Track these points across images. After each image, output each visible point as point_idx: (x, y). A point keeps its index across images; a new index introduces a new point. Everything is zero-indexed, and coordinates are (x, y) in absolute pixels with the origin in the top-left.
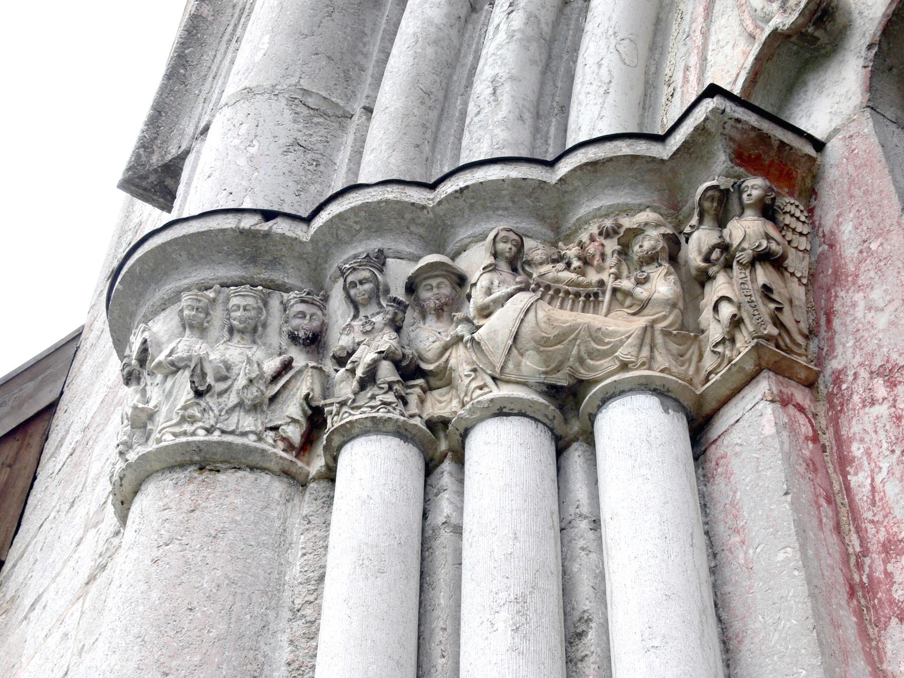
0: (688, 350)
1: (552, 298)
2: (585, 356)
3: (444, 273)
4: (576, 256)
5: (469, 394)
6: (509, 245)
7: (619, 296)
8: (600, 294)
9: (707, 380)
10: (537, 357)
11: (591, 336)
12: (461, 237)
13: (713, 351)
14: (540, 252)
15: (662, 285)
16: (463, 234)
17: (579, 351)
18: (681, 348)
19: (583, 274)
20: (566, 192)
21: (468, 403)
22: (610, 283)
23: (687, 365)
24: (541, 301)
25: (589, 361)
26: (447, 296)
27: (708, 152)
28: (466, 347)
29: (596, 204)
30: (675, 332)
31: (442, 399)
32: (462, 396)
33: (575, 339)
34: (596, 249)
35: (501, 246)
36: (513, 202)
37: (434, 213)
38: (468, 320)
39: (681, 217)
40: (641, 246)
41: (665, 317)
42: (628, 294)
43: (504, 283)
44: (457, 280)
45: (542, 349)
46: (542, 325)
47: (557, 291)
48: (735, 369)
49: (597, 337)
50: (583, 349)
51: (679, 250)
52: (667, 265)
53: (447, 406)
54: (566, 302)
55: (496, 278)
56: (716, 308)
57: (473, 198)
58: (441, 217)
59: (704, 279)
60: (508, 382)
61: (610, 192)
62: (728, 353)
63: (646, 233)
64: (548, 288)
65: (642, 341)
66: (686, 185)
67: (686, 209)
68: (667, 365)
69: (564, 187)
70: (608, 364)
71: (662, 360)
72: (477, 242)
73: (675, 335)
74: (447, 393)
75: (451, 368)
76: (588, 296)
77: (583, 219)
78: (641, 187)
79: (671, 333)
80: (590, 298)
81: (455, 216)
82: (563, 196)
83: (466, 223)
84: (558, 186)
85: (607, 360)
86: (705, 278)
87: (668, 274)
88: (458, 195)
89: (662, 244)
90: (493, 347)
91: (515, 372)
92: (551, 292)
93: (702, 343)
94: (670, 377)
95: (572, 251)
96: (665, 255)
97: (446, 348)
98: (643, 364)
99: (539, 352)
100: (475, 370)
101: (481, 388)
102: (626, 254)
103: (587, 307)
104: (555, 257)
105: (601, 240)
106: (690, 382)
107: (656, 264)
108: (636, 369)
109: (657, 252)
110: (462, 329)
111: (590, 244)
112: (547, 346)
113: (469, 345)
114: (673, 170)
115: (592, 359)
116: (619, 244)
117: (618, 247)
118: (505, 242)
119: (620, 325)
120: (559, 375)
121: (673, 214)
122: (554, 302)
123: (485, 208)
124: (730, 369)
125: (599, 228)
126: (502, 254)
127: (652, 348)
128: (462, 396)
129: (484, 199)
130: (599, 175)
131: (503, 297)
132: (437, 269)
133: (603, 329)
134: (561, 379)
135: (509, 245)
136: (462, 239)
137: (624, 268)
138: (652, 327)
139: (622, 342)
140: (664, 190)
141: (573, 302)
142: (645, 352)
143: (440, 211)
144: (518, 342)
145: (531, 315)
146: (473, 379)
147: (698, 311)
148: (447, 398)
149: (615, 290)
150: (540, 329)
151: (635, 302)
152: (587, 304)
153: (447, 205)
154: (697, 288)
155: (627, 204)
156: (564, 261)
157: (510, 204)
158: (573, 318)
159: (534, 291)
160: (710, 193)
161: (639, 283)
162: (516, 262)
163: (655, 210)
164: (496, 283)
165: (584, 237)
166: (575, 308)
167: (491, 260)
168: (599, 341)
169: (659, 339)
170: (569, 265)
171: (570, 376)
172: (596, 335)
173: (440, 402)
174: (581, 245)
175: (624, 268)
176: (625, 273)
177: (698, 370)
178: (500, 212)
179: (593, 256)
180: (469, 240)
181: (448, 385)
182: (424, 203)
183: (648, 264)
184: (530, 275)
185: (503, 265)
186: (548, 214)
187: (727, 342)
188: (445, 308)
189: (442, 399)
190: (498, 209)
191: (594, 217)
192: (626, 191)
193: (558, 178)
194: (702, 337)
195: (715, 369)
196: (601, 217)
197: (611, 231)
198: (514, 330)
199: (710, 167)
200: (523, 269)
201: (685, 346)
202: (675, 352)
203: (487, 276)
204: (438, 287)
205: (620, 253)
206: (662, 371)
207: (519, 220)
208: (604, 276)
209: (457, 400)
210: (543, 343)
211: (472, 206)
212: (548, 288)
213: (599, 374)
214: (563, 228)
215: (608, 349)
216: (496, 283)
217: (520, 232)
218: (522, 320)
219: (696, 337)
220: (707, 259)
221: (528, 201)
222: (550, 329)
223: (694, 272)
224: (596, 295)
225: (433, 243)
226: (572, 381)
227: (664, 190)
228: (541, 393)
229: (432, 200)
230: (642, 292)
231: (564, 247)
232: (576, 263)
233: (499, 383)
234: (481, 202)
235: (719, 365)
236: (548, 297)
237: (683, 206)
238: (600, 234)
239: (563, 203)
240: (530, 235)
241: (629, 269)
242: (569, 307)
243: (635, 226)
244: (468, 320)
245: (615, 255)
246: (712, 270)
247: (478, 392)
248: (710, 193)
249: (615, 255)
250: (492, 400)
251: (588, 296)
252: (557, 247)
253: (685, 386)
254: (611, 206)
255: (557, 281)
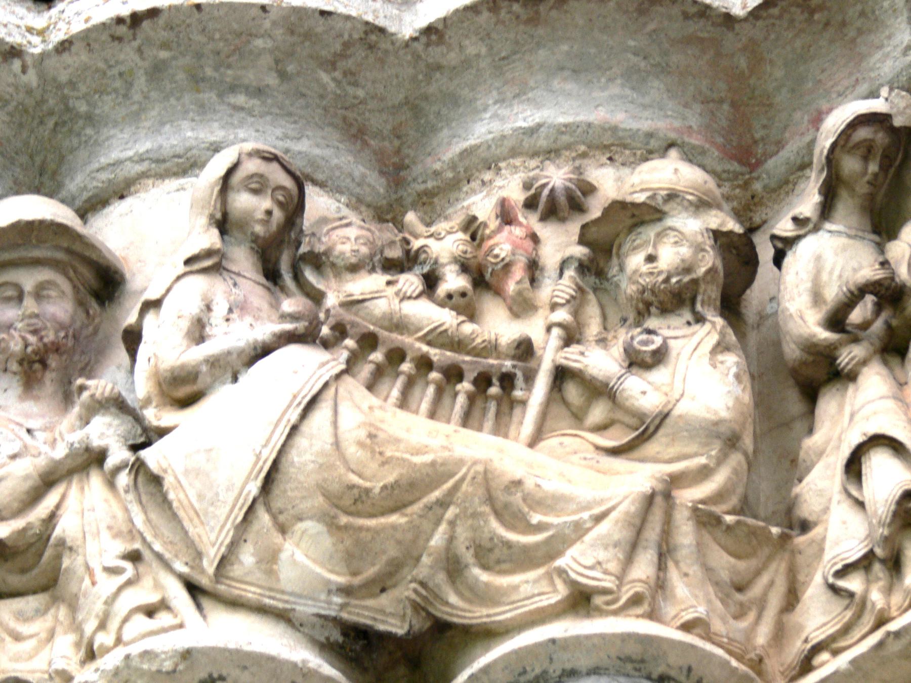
0: (758, 573)
1: (379, 373)
2: (468, 557)
3: (60, 255)
4: (455, 260)
5: (113, 625)
6: (266, 203)
7: (572, 392)
8: (520, 381)
9: (806, 666)
10: (327, 542)
11: (490, 499)
12: (115, 155)
13: (834, 589)
14: (352, 232)
15: (700, 376)
16: (124, 147)
17: (451, 539)
18: (742, 565)
19: (472, 315)
20: (439, 67)
21: (106, 650)
22: (550, 353)
23: (752, 616)
24: (348, 379)
25: (476, 571)
26: (61, 326)
27: (862, 14)
28: (111, 483)
29: (524, 116)
30: (729, 519)
31: (24, 629)
32: (90, 627)
33: (443, 504)
34: (516, 247)
35: (243, 201)
36: (283, 75)
37: (41, 76)
38: (119, 405)
39: (757, 186)
40: (651, 259)
41: (704, 473)
42: (599, 390)
43: (244, 313)
44: (93, 282)
45: (344, 520)
46: (352, 451)
47: (397, 356)
48: (895, 647)
49: (507, 506)
50: (463, 534)
51: (749, 280)
52: (720, 321)
53: (36, 651)
54: (417, 391)
55: (219, 290)
56: (854, 467)
57: (165, 46)
58: (60, 87)
59: (817, 376)
60: (235, 604)
61: (570, 86)
62: (876, 597)
63: (669, 222)
64: (369, 341)
65: (639, 532)
66: (782, 98)
67: (775, 165)
68: (701, 611)
69: (436, 53)
70: (530, 588)
71: (689, 597)
72: (162, 176)
73: (729, 528)
74: (41, 613)
75: (62, 543)
76: (483, 381)
77: (483, 153)
78: (656, 87)
79: (718, 520)
80: (489, 387)
81: (101, 92)
82: (429, 78)
83: (135, 117)
84: (419, 47)
85: (532, 575)
86: (821, 373)
87: (721, 347)
88: (122, 30)
89: (709, 260)
90: (201, 497)
91: (258, 577)
92: (377, 354)
93: (800, 559)
94: (708, 647)
95: (444, 244)
96: (714, 292)
97: (48, 480)
98: (636, 600)
99: (333, 526)
100: (134, 557)
101: (150, 612)
102: (600, 274)
103: (476, 413)
104: (395, 253)
105: (532, 221)
106: (758, 664)
107: (688, 316)
108: (615, 613)
109: (695, 282)
110: (106, 432)
111: (499, 230)
112: (358, 514)
113: (124, 479)
114: (752, 49)
115: (485, 567)
116: (582, 241)
117: (580, 251)
118: (255, 192)
119: (574, 477)
120: (384, 600)
121: (736, 175)
122: (383, 387)
123: (197, 80)
124: (880, 645)
125: (527, 186)
126: (243, 224)
127: (665, 554)
128: (90, 627)
129: (199, 55)
130: (541, 31)
131: (241, 352)
132: (40, 242)
133: (529, 484)
134: (390, 616)
135: (266, 203)
136: (118, 163)
137: (592, 313)
138: (668, 496)
139: (579, 531)
140: (721, 101)
141: (440, 391)
142: (643, 568)
143: (63, 70)
144: (276, 491)
145: (321, 416)
146: (129, 583)
147: (793, 467)
148: (39, 626)
149: (562, 375)
150: (345, 461)
151: (619, 415)
152: (479, 403)
153: (84, 57)
154: (794, 403)
155: (614, 129)
156: (418, 270)
157: (272, 80)
158: (441, 441)
159: (326, 345)
160: (863, 133)
161: (637, 362)
162: (281, 255)
163: (691, 156)
164: (220, 308)
165: (482, 205)
166: (442, 412)
167: (211, 239)
168: (513, 518)
169: (686, 534)
170: (431, 281)
171: (417, 607)
172: (505, 500)
173: (17, 637)
174: (473, 229)
175: (592, 313)
176: (593, 328)
177: (780, 635)
178: (240, 99)
179: (507, 267)
180: (139, 168)
181: (44, 589)
182: (16, 38)
183: (665, 311)
184: (317, 297)
185: (243, 260)
186: (376, 122)
187: (877, 567)
188: (53, 361)
189: (24, 629)
190: (233, 88)
191: (514, 153)
192: (615, 89)
193: (423, 23)
194: (801, 540)
195: (833, 638)
196: (534, 154)
197: (562, 200)
198: (269, 455)
199: (862, 57)
200: (297, 277)
201: (753, 563)
202: (725, 575)
203: (198, 284)
204: (39, 294)
205: (583, 268)
206: (687, 627)
207: (291, 130)
208: (533, 328)
209: (72, 638)
210: (347, 504)
211: (157, 71)
212: (369, 341)
213: (502, 614)
214: (417, 170)
215: (537, 546)
216: (220, 308)
217: (297, 165)
218: (294, 429)
219: (785, 538)
220: (836, 321)
221: (325, 77)
222: (373, 466)
223: (792, 352)
224: (507, 380)
225: (24, 159)
226: (420, 624)
227: (721, 101)
228: (326, 648)
229: (41, 33)
230: (643, 392)
231: (421, 228)
232: (454, 281)
233: (206, 603)
234: (187, 60)
235: (846, 630)
236: (366, 370)
237: (768, 156)
238: (530, 204)
239: (426, 98)
240: (320, 176)
241: (604, 317)
242: (425, 406)
243: (640, 198)
244: (119, 405)
245: (570, 273)
246: (848, 356)
247: (141, 623)
248: (863, 133)
249: (570, 273)
250: (187, 654)
251: (483, 381)
252: (400, 225)
253: (746, 677)
254: (567, 128)
255: (399, 325)
